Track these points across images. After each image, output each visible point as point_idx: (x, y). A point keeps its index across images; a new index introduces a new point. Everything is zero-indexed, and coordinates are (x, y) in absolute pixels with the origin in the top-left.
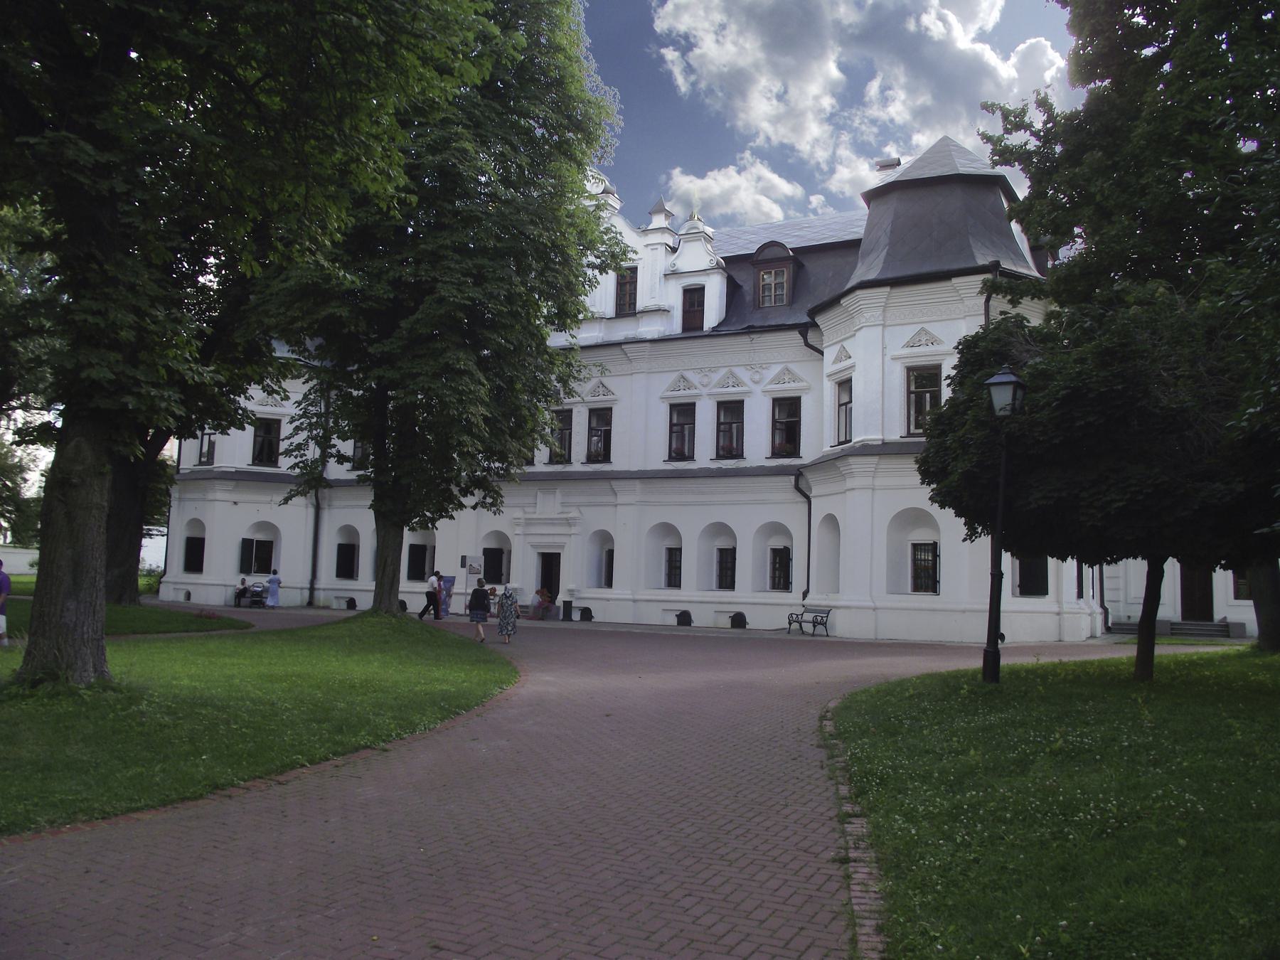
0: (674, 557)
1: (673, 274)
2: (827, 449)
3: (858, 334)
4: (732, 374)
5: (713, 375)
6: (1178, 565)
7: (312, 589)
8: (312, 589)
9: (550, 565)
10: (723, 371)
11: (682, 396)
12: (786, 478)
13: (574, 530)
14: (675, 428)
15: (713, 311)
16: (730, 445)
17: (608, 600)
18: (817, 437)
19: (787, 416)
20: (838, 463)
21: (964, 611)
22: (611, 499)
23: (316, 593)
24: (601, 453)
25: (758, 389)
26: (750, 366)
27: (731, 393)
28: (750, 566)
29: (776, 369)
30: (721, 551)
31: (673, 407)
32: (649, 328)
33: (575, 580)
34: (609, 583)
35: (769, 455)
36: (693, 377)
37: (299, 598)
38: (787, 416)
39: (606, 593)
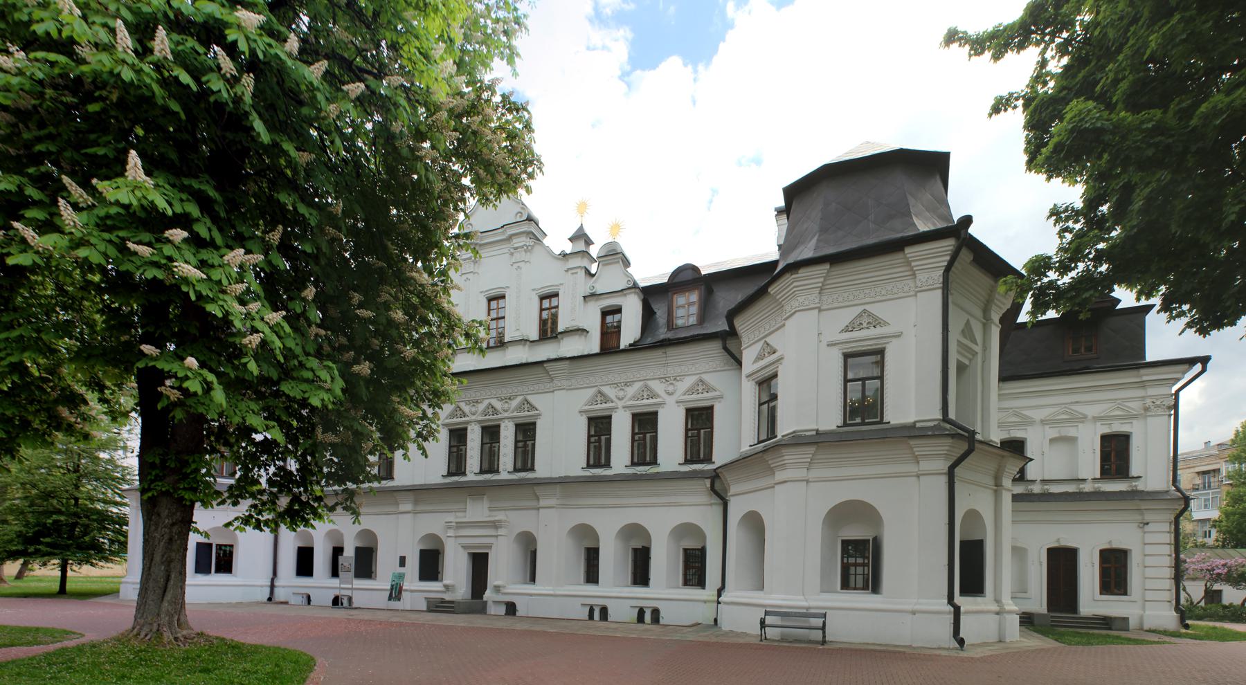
0: (592, 556)
1: (591, 296)
2: (745, 448)
3: (788, 323)
4: (646, 386)
7: (272, 587)
8: (272, 587)
9: (479, 563)
10: (637, 386)
11: (600, 409)
12: (700, 482)
13: (501, 532)
14: (592, 439)
15: (630, 330)
16: (644, 449)
17: (531, 595)
18: (733, 436)
19: (700, 420)
20: (766, 457)
21: (914, 613)
22: (534, 503)
23: (276, 590)
24: (525, 457)
25: (671, 401)
26: (664, 379)
27: (645, 405)
28: (664, 562)
29: (689, 382)
30: (635, 550)
31: (590, 420)
32: (570, 347)
33: (503, 574)
34: (533, 579)
35: (682, 461)
36: (610, 392)
38: (700, 420)
39: (530, 589)
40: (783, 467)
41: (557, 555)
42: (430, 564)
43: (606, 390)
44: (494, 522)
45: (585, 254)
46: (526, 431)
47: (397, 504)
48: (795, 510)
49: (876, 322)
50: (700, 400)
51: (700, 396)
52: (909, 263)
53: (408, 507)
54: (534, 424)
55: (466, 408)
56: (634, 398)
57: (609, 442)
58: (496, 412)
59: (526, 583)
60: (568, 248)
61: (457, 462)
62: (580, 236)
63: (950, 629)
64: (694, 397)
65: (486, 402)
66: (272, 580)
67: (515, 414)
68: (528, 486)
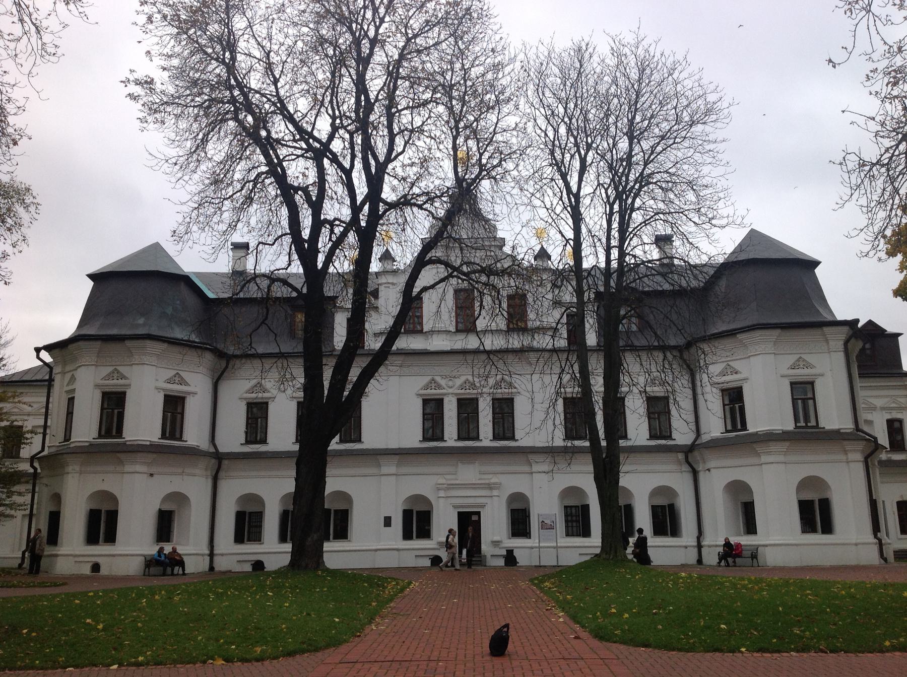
5: (456, 380)
6: (290, 558)
7: (212, 555)
13: (495, 493)
17: (114, 556)
22: (526, 468)
23: (216, 559)
33: (494, 530)
37: (204, 565)
40: (769, 453)
43: (438, 379)
44: (489, 484)
47: (379, 466)
48: (776, 486)
49: (808, 366)
51: (115, 381)
52: (824, 335)
53: (393, 469)
54: (124, 393)
55: (443, 382)
57: (121, 416)
64: (463, 391)
65: (463, 379)
66: (698, 538)
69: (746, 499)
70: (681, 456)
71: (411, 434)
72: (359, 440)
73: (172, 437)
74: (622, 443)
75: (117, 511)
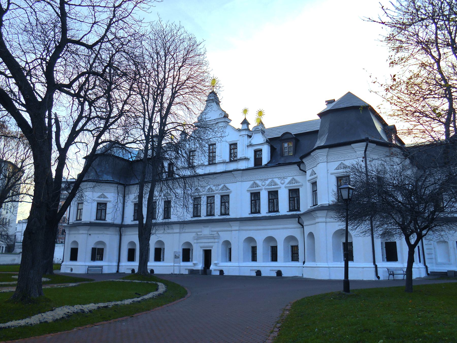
0: (254, 250)
1: (251, 145)
4: (273, 181)
5: (285, 180)
7: (118, 266)
8: (118, 266)
9: (207, 254)
11: (255, 189)
13: (216, 240)
15: (266, 158)
19: (294, 194)
23: (120, 267)
24: (225, 210)
25: (283, 186)
27: (273, 188)
29: (289, 179)
32: (242, 165)
34: (230, 260)
38: (294, 194)
39: (229, 264)
41: (239, 248)
42: (187, 255)
43: (258, 182)
45: (248, 129)
46: (225, 199)
50: (294, 186)
51: (294, 184)
53: (178, 231)
55: (214, 188)
56: (268, 185)
58: (213, 191)
59: (227, 262)
60: (240, 127)
61: (196, 213)
62: (245, 122)
63: (374, 274)
64: (291, 185)
67: (221, 192)
68: (226, 220)
69: (273, 245)
70: (118, 228)
71: (246, 212)
72: (278, 211)
73: (255, 213)
74: (154, 221)
75: (277, 247)
